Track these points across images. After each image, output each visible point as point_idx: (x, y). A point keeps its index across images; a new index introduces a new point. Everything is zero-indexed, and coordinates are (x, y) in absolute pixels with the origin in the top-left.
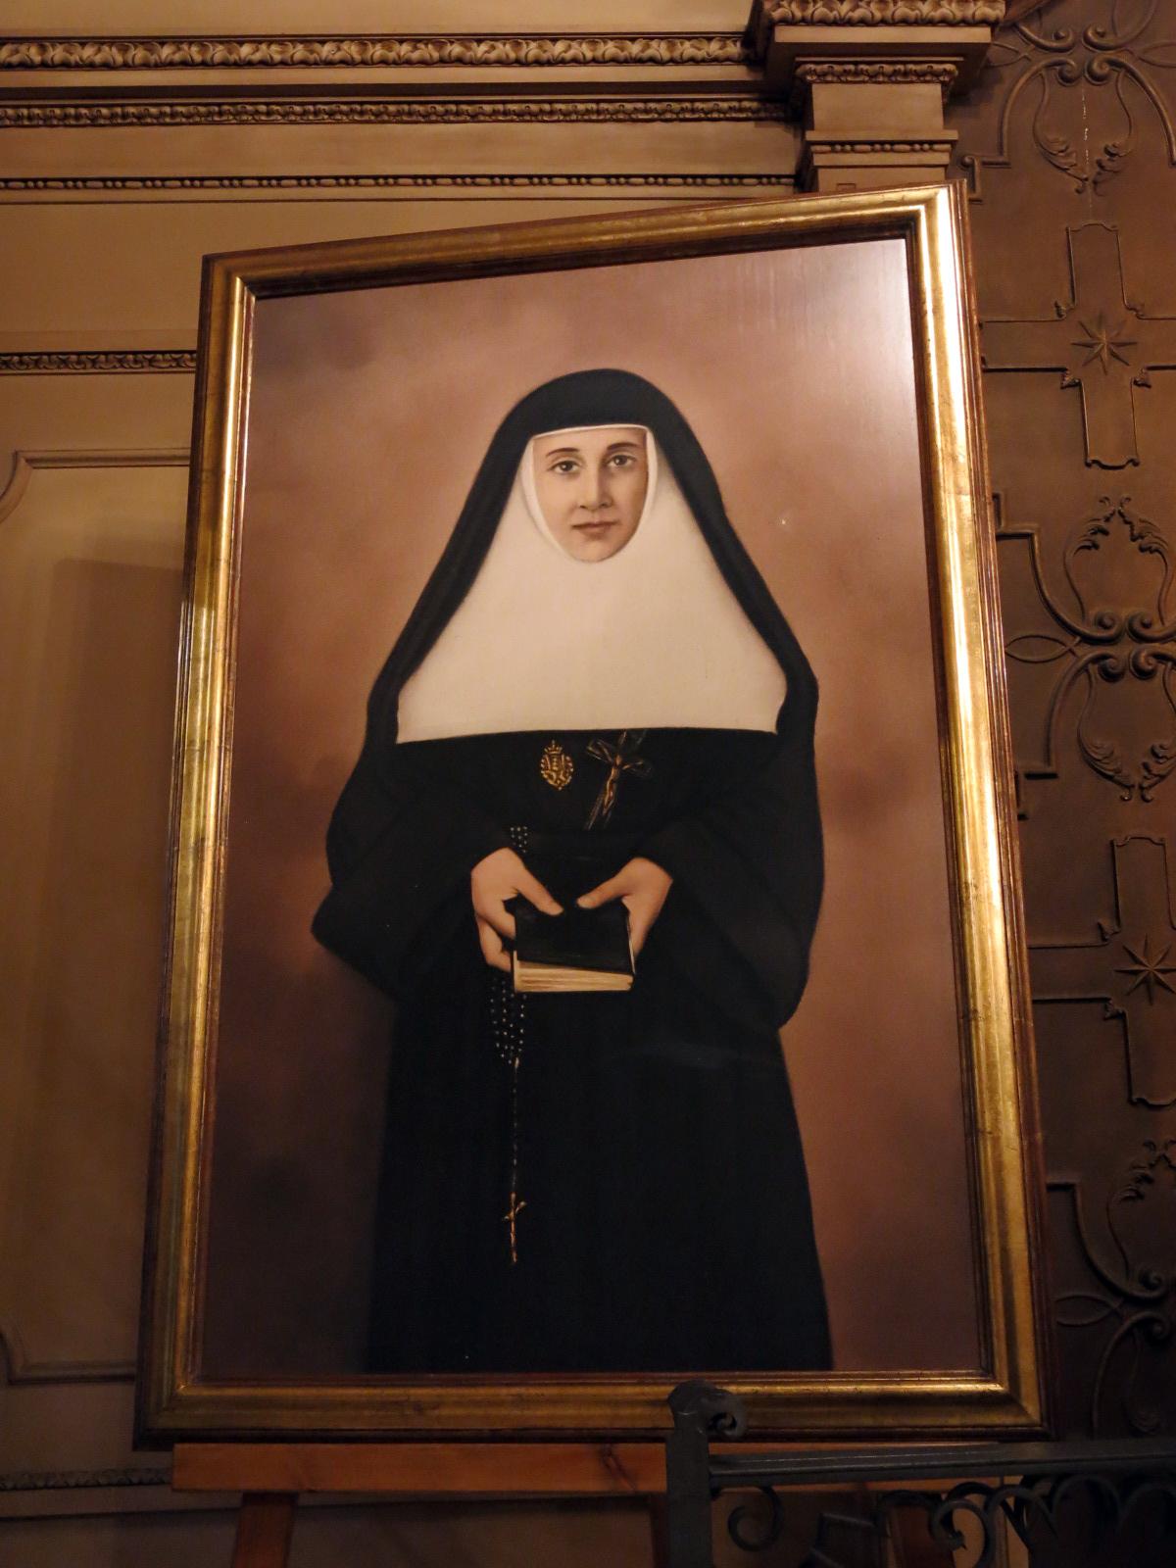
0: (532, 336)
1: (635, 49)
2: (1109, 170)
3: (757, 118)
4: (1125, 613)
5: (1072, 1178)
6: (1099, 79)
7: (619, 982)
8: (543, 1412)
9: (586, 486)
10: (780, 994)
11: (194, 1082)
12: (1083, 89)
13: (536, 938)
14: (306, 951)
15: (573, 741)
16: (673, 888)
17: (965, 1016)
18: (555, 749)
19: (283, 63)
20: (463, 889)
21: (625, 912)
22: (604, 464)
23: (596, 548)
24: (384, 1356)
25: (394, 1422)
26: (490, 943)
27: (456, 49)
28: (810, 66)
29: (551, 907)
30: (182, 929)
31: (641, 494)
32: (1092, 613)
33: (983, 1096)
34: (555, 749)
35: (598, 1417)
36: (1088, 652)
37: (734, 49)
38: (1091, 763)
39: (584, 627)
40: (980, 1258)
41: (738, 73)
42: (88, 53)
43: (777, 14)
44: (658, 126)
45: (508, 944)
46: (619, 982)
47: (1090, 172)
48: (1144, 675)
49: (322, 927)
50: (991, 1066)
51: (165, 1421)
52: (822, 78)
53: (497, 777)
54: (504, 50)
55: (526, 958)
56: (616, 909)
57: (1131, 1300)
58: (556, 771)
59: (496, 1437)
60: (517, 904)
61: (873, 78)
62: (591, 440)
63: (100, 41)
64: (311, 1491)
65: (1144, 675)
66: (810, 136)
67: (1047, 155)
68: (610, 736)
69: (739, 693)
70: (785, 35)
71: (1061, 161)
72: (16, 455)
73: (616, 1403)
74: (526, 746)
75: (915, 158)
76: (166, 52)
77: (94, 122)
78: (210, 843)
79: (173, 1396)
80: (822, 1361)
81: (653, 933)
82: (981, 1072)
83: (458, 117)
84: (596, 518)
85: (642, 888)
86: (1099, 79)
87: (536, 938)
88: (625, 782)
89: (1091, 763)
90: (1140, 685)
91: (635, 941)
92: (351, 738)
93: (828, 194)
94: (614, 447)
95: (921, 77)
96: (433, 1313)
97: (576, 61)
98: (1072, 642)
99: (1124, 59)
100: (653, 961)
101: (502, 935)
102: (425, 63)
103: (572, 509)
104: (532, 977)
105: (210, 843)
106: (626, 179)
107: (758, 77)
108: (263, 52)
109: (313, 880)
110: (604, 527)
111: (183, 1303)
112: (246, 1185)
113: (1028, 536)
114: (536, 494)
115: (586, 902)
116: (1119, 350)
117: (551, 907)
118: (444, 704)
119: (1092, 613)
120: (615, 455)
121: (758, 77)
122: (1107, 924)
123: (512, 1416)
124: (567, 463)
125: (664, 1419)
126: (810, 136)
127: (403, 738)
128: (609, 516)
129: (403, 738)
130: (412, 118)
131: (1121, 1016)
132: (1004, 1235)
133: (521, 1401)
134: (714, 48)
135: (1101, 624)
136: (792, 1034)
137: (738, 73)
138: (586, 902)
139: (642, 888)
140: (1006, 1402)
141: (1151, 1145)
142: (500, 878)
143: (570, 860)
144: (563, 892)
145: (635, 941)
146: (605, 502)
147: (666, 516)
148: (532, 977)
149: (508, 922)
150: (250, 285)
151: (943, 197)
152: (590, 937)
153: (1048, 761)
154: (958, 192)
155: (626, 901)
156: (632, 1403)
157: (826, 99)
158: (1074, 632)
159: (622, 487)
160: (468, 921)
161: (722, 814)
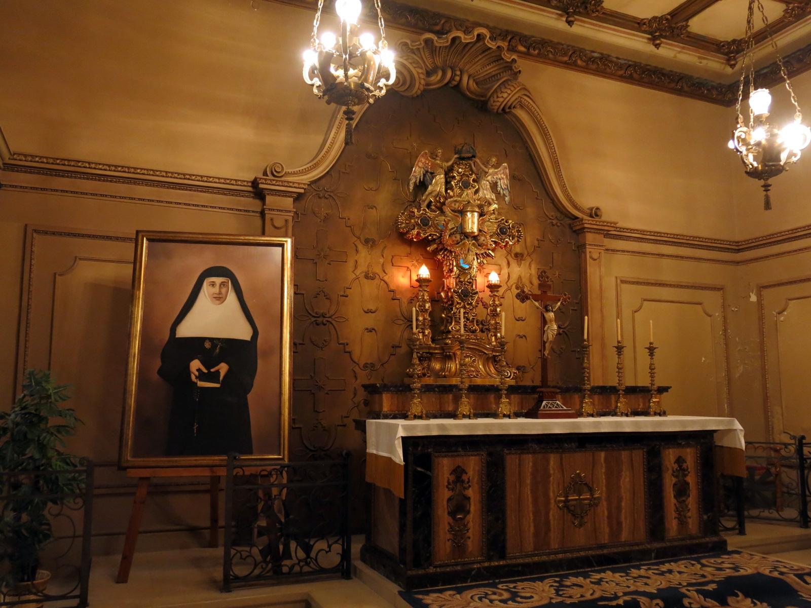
0: (206, 258)
1: (228, 181)
2: (327, 218)
3: (253, 198)
4: (322, 312)
5: (301, 426)
6: (327, 198)
7: (218, 385)
8: (199, 462)
9: (216, 290)
10: (248, 388)
11: (132, 402)
12: (323, 199)
13: (202, 376)
14: (155, 377)
15: (211, 340)
16: (229, 369)
17: (281, 393)
18: (207, 341)
19: (147, 174)
20: (188, 367)
21: (219, 373)
22: (220, 285)
23: (218, 302)
24: (168, 453)
25: (171, 464)
26: (193, 378)
27: (188, 177)
28: (266, 192)
29: (205, 371)
30: (130, 371)
31: (227, 292)
32: (315, 311)
33: (282, 408)
34: (207, 341)
35: (210, 463)
36: (313, 319)
37: (250, 184)
38: (312, 342)
39: (213, 317)
40: (280, 435)
41: (250, 189)
42: (100, 166)
43: (260, 182)
44: (231, 197)
45: (197, 378)
46: (218, 385)
47: (323, 218)
48: (325, 325)
49: (160, 372)
50: (284, 402)
51: (124, 465)
52: (268, 194)
53: (196, 346)
54: (199, 178)
55: (201, 380)
56: (218, 372)
57: (311, 450)
58: (207, 345)
59: (190, 466)
60: (199, 370)
61: (279, 196)
62: (218, 280)
63: (104, 165)
64: (154, 477)
65: (325, 325)
66: (265, 207)
67: (314, 213)
68: (219, 339)
69: (243, 332)
70: (261, 186)
71: (318, 215)
72: (76, 257)
73: (214, 460)
74: (202, 340)
75: (287, 214)
76: (119, 169)
77: (99, 180)
78: (136, 355)
79: (127, 460)
80: (251, 453)
81: (224, 377)
82: (282, 405)
83: (186, 190)
84: (218, 296)
85: (223, 368)
86: (327, 198)
87: (202, 376)
88: (221, 347)
89: (312, 342)
90: (322, 326)
91: (221, 378)
92: (166, 336)
93: (268, 236)
94: (222, 282)
95: (289, 197)
96: (179, 443)
97: (215, 182)
98: (310, 317)
99: (332, 194)
100: (223, 383)
101: (195, 375)
102: (180, 178)
103: (214, 294)
104: (201, 384)
105: (136, 355)
106: (224, 208)
107: (255, 190)
108: (143, 172)
109: (157, 364)
110: (219, 298)
111: (129, 443)
112: (143, 422)
113: (303, 294)
114: (206, 290)
115: (212, 370)
116: (325, 257)
117: (205, 371)
118: (186, 330)
119: (315, 311)
120: (222, 284)
121: (255, 190)
122: (313, 375)
123: (194, 463)
124: (213, 284)
125: (224, 463)
126: (265, 207)
127: (177, 337)
128: (220, 296)
129: (177, 337)
130: (176, 189)
131: (313, 394)
132: (284, 431)
133: (196, 460)
134: (245, 183)
135: (316, 313)
136: (250, 397)
137: (250, 189)
138: (212, 370)
139: (223, 368)
140: (283, 459)
141: (317, 420)
142: (196, 365)
143: (208, 363)
144: (208, 368)
145: (221, 378)
146: (220, 293)
147: (232, 297)
148: (201, 384)
149: (197, 373)
150: (147, 239)
151: (289, 240)
152: (214, 377)
153: (303, 340)
154: (292, 240)
155: (220, 371)
156: (217, 460)
157: (269, 199)
158: (311, 315)
159: (224, 290)
160: (188, 372)
161: (238, 354)
